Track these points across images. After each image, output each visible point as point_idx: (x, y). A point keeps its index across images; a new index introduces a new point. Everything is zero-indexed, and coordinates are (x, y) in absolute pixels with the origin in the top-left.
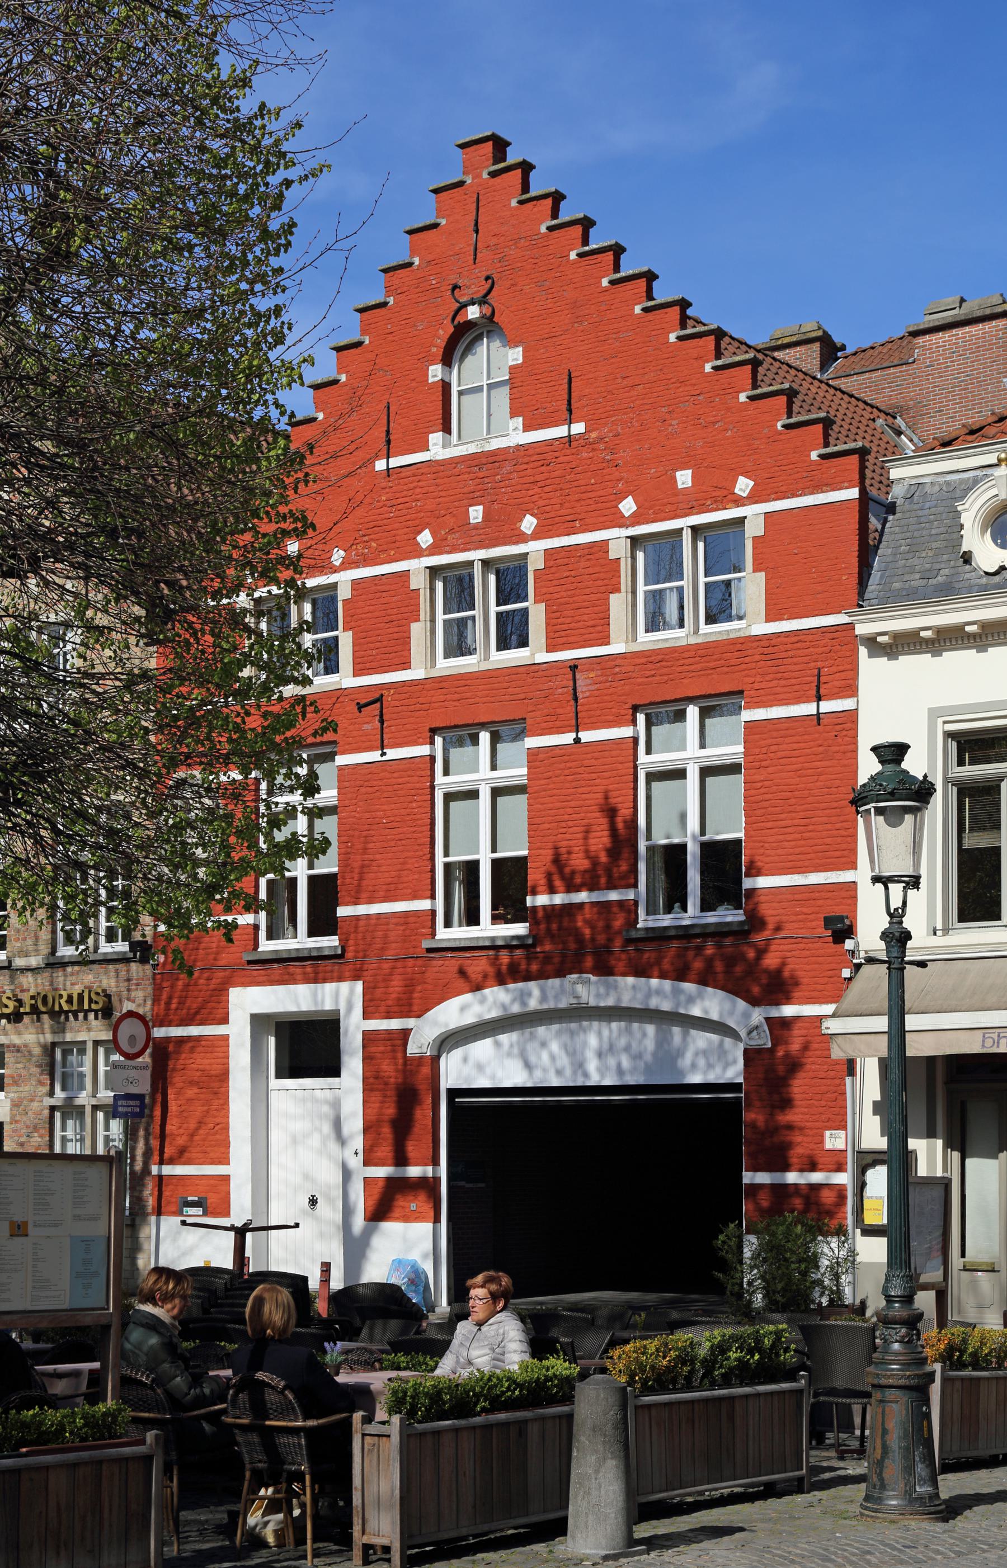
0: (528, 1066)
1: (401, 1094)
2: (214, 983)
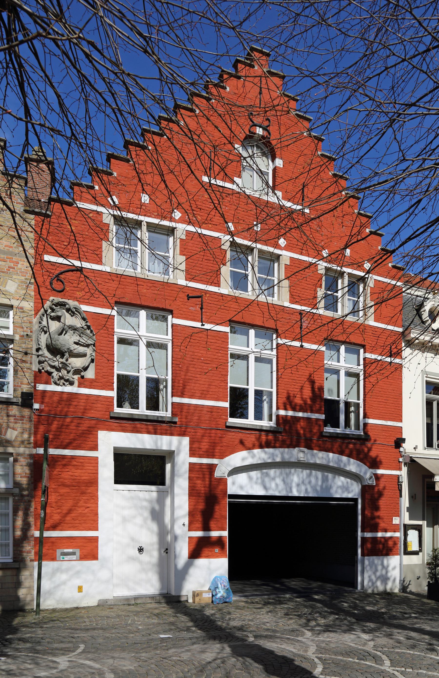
0: (265, 488)
1: (207, 496)
2: (83, 427)
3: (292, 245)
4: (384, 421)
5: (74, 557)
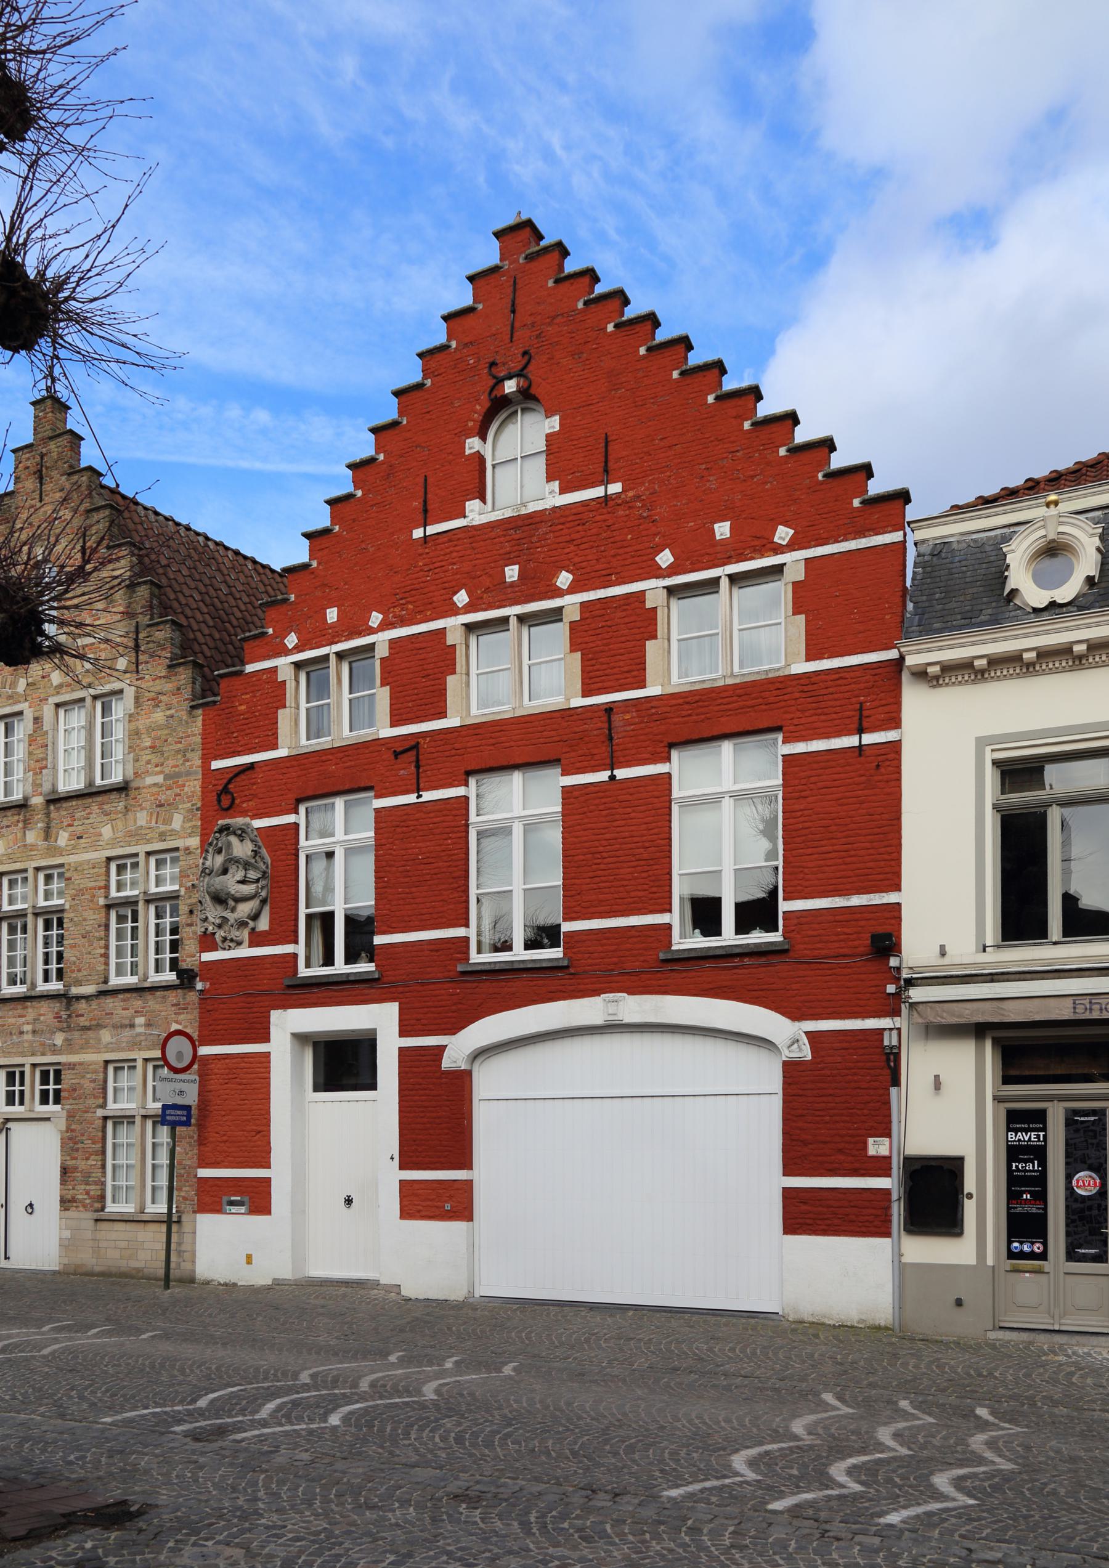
3: (586, 577)
4: (837, 899)
5: (242, 1209)
